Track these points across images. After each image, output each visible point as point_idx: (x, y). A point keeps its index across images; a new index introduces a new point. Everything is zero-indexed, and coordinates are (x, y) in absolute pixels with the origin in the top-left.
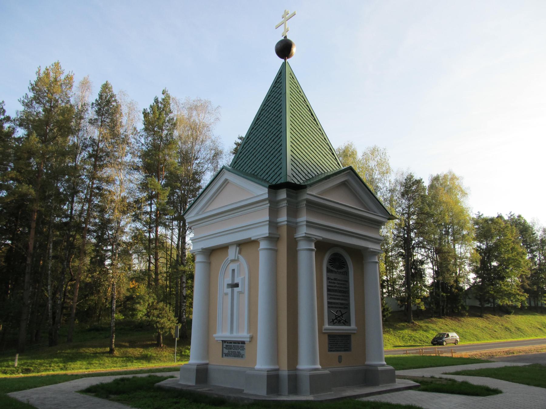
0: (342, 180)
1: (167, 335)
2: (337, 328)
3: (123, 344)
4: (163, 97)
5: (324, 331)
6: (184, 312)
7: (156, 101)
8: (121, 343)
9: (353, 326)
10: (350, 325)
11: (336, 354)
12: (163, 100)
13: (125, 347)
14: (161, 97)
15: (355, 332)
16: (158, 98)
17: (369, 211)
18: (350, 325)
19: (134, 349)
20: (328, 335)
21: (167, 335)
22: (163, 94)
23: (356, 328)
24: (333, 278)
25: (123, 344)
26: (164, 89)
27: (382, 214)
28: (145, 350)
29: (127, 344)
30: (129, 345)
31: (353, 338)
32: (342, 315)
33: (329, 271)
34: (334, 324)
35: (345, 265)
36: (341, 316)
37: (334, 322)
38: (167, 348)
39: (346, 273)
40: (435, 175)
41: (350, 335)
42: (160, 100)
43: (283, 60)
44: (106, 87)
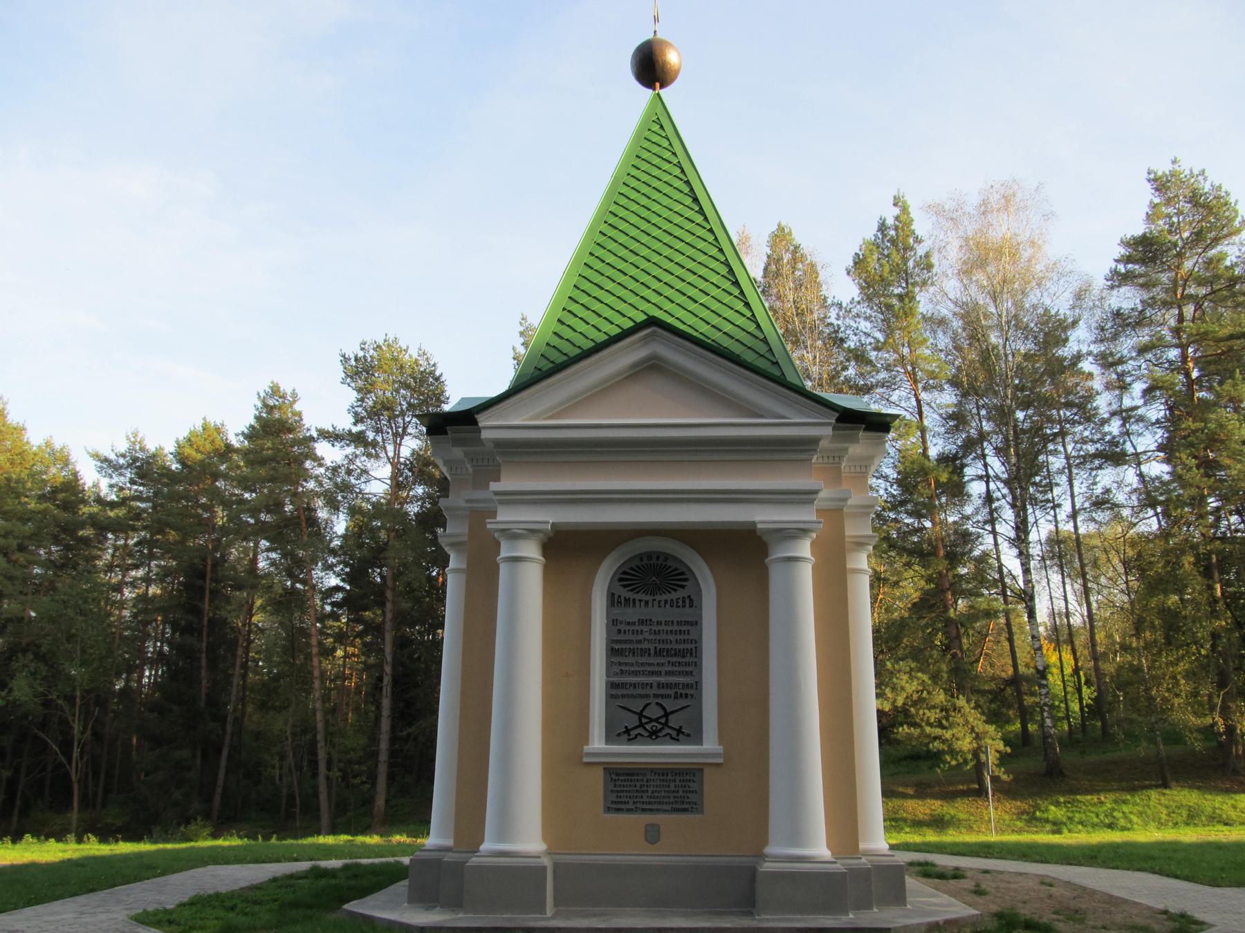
0: (642, 353)
1: (968, 767)
2: (667, 752)
3: (901, 789)
4: (896, 211)
5: (585, 760)
6: (1045, 711)
7: (883, 227)
8: (895, 788)
9: (710, 744)
10: (700, 742)
11: (637, 821)
12: (897, 218)
13: (904, 796)
14: (890, 213)
15: (720, 760)
16: (885, 219)
17: (762, 416)
18: (700, 742)
19: (920, 803)
20: (605, 769)
21: (968, 767)
22: (895, 205)
23: (719, 749)
24: (636, 620)
25: (901, 789)
26: (895, 193)
27: (809, 417)
28: (946, 804)
29: (910, 791)
30: (916, 791)
31: (709, 776)
32: (666, 715)
33: (613, 601)
34: (629, 740)
35: (686, 580)
36: (640, 720)
37: (629, 735)
38: (1003, 801)
39: (693, 602)
40: (1144, 216)
41: (702, 770)
42: (890, 221)
43: (648, 93)
44: (780, 237)
